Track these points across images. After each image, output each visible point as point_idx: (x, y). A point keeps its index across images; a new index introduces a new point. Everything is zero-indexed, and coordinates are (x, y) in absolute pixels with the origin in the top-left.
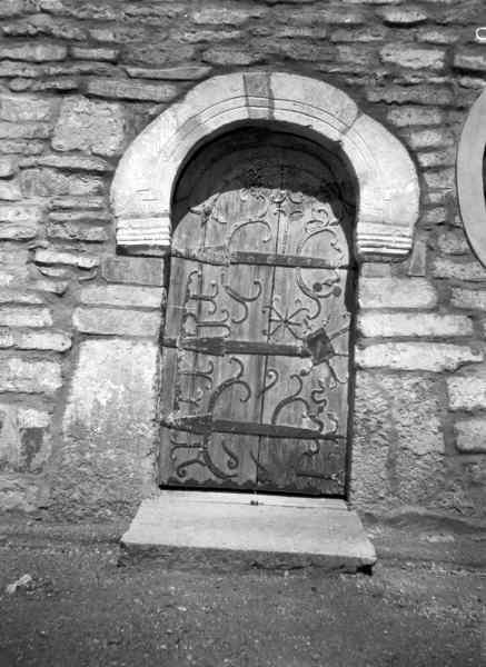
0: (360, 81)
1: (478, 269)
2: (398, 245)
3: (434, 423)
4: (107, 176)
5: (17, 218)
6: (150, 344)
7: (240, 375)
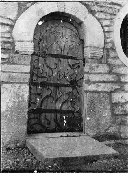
0: (89, 3)
1: (119, 61)
2: (100, 54)
3: (109, 107)
4: (12, 26)
5: (123, 95)
6: (27, 85)
7: (50, 94)
